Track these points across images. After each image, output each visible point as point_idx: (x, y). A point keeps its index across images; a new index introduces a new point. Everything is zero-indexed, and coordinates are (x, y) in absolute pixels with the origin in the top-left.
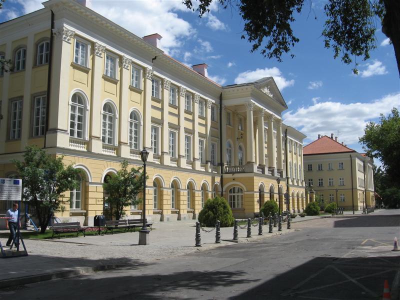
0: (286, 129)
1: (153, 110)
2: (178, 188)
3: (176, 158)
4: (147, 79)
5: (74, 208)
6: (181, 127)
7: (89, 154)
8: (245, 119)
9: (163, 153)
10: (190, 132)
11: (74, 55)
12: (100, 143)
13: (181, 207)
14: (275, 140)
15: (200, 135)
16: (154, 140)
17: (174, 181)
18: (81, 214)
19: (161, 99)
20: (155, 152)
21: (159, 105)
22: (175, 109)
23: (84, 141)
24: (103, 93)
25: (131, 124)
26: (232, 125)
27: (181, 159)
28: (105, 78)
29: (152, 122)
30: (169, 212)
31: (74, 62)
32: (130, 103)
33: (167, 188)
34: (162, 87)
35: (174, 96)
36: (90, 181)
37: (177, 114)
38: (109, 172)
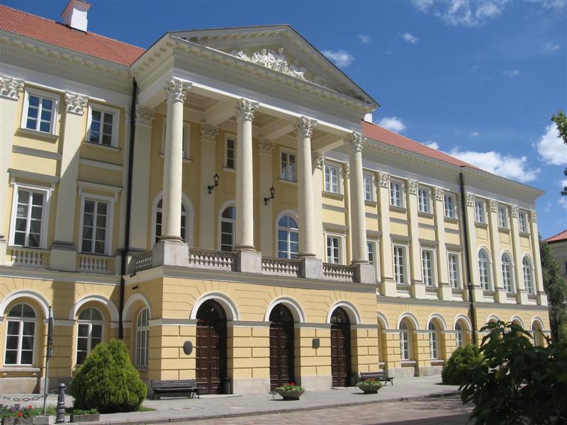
0: (461, 174)
1: (421, 229)
3: (460, 289)
4: (381, 188)
6: (440, 244)
8: (298, 159)
9: (440, 284)
10: (429, 248)
13: (420, 357)
15: (449, 247)
16: (427, 269)
17: (535, 322)
18: (29, 374)
19: (432, 213)
20: (530, 292)
21: (431, 222)
24: (501, 245)
25: (480, 263)
28: (500, 230)
29: (368, 237)
30: (399, 366)
32: (501, 245)
33: (449, 331)
34: (377, 185)
35: (523, 222)
36: (387, 328)
37: (406, 219)
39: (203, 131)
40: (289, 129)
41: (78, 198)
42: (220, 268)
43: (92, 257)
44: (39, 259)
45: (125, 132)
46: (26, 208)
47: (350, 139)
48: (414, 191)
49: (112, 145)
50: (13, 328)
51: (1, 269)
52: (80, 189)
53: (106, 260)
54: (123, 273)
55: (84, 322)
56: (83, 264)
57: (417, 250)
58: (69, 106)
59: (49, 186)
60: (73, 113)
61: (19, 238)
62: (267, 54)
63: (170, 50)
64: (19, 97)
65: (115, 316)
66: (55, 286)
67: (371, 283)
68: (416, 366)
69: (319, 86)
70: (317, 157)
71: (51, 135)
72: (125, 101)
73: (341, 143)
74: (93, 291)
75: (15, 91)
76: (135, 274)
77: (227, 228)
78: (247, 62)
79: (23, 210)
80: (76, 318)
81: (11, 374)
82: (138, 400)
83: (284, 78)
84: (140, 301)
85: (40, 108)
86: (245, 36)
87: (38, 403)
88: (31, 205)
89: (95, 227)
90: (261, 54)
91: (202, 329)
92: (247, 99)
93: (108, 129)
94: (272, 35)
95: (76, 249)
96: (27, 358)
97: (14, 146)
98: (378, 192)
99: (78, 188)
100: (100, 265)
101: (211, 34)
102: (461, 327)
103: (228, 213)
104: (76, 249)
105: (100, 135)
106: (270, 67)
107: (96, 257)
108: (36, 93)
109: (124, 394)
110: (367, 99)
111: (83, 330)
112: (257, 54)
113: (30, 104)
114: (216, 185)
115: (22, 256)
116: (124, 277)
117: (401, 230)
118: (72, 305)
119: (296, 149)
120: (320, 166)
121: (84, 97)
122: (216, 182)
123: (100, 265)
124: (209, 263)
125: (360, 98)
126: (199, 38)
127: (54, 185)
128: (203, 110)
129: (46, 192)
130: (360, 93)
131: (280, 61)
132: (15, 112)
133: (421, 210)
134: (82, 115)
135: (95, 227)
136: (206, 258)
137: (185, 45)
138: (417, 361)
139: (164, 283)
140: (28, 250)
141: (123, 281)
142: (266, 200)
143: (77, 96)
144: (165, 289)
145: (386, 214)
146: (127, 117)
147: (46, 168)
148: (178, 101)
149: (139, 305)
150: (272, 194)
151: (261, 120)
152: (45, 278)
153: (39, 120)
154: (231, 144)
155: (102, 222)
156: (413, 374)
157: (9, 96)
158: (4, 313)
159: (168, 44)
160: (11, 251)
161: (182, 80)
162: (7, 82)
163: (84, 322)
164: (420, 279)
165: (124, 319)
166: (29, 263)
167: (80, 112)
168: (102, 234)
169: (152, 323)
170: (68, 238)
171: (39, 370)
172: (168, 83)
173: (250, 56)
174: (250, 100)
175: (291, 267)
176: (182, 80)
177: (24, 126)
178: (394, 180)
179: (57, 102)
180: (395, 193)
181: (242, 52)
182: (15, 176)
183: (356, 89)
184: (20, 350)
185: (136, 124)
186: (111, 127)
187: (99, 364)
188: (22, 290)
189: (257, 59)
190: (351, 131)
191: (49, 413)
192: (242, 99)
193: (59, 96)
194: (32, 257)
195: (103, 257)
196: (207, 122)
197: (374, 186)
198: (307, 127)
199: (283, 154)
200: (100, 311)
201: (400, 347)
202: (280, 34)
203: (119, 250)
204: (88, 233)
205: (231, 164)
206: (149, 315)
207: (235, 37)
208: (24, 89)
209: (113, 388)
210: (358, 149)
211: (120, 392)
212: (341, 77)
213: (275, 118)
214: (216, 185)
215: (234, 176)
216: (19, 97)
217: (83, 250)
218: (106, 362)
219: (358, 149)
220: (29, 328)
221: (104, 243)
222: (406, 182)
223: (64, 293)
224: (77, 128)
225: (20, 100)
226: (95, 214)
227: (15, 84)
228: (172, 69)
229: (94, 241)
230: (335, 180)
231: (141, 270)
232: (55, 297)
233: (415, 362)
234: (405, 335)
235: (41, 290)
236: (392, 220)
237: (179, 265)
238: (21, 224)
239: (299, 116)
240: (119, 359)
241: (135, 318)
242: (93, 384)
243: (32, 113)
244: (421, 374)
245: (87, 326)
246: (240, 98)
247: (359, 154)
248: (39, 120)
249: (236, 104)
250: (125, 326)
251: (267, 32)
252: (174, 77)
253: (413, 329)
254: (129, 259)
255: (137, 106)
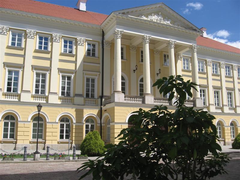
2: (236, 126)
4: (221, 69)
5: (232, 138)
7: (20, 103)
11: (183, 65)
12: (214, 107)
13: (226, 137)
14: (191, 66)
18: (12, 142)
22: (218, 77)
23: (206, 107)
26: (125, 59)
27: (224, 107)
31: (183, 69)
34: (206, 65)
37: (220, 79)
38: (233, 121)
39: (155, 52)
40: (165, 45)
41: (83, 77)
42: (137, 102)
43: (89, 99)
44: (70, 101)
45: (100, 51)
46: (65, 82)
47: (191, 48)
48: (223, 67)
49: (95, 56)
50: (6, 124)
51: (1, 102)
52: (84, 74)
53: (95, 101)
54: (101, 105)
55: (87, 124)
56: (86, 102)
57: (211, 91)
58: (78, 43)
59: (73, 73)
60: (30, 38)
61: (63, 93)
62: (154, 16)
63: (114, 18)
64: (60, 41)
65: (99, 121)
66: (76, 111)
67: (201, 107)
68: (224, 141)
69: (177, 27)
70: (179, 55)
71: (204, 72)
72: (99, 39)
73: (188, 49)
74: (90, 112)
75: (32, 35)
76: (105, 106)
77: (142, 86)
78: (146, 20)
79: (64, 83)
80: (84, 122)
81: (5, 142)
82: (103, 152)
83: (153, 23)
84: (108, 116)
85: (43, 41)
86: (144, 10)
87: (66, 153)
88: (66, 81)
89: (90, 88)
90: (152, 16)
91: (131, 126)
92: (172, 40)
93: (94, 50)
94: (156, 7)
95: (83, 97)
96: (67, 137)
97: (59, 59)
98: (207, 68)
99: (83, 73)
100: (93, 102)
101: (130, 10)
102: (234, 124)
103: (142, 80)
104: (83, 97)
105: (90, 53)
106: (155, 21)
107: (91, 99)
108: (66, 39)
109: (98, 150)
110: (198, 30)
111: (87, 127)
112: (150, 16)
113: (39, 40)
114: (136, 69)
115: (64, 100)
116: (102, 106)
117: (218, 84)
118: (83, 117)
119: (168, 52)
120: (180, 59)
121: (84, 39)
122: (136, 68)
123: (93, 102)
124: (161, 102)
125: (195, 30)
126: (125, 13)
127: (74, 73)
128: (130, 40)
129: (72, 76)
130: (195, 28)
131: (159, 18)
132: (7, 39)
133: (226, 74)
134: (83, 46)
135: (90, 88)
136: (135, 99)
137: (120, 16)
138: (225, 139)
139: (115, 109)
140: (90, 99)
141: (101, 108)
142: (157, 74)
143: (81, 39)
144: (116, 111)
145: (210, 77)
146: (101, 45)
147: (71, 67)
148: (118, 38)
149: (107, 118)
150: (160, 72)
151: (153, 42)
152: (72, 108)
153: (43, 45)
154: (142, 52)
155: (93, 86)
156: (223, 145)
157: (56, 41)
158: (59, 121)
159: (113, 16)
160: (60, 98)
161: (120, 30)
162: (55, 36)
163: (87, 124)
164: (226, 104)
165: (102, 122)
166: (65, 102)
167: (83, 45)
168: (93, 91)
169: (111, 124)
170: (80, 92)
171: (71, 141)
172: (114, 31)
173: (147, 17)
174: (148, 35)
175: (163, 101)
176: (120, 30)
177: (37, 48)
178: (214, 62)
179: (23, 34)
180: (214, 68)
181: (143, 16)
182: (6, 65)
183: (193, 27)
184: (65, 134)
185: (104, 47)
186: (95, 49)
187: (89, 139)
188: (64, 112)
189: (150, 18)
190: (191, 44)
191: (70, 156)
192: (170, 40)
193: (24, 32)
194: (68, 100)
195: (89, 99)
196: (132, 45)
197: (205, 66)
198: (172, 44)
199: (164, 55)
200: (94, 120)
201: (231, 133)
202: (159, 7)
203: (99, 96)
204: (88, 91)
205: (142, 61)
206: (110, 121)
207: (140, 10)
208: (62, 38)
209: (94, 148)
210: (195, 51)
211: (96, 149)
212: (186, 22)
213: (135, 37)
214: (136, 69)
215: (142, 65)
216: (60, 41)
217: (86, 97)
218: (91, 138)
219: (195, 51)
220: (68, 126)
221: (94, 94)
222: (219, 63)
223: (79, 113)
224: (82, 51)
225: (61, 42)
226: (90, 83)
227: (58, 36)
228: (116, 26)
229: (90, 93)
230: (187, 64)
231: (107, 104)
232: (76, 114)
233: (224, 139)
234: (233, 128)
235: (71, 112)
236: (226, 81)
237: (121, 102)
238: (63, 88)
239: (169, 40)
240: (96, 137)
241: (106, 121)
242: (87, 146)
243: (41, 43)
244: (226, 144)
245: (89, 125)
246: (143, 34)
247: (195, 54)
248: (43, 45)
249: (142, 37)
250: (102, 125)
251: (153, 6)
252: (117, 29)
253: (223, 125)
254: (103, 100)
255: (104, 40)
